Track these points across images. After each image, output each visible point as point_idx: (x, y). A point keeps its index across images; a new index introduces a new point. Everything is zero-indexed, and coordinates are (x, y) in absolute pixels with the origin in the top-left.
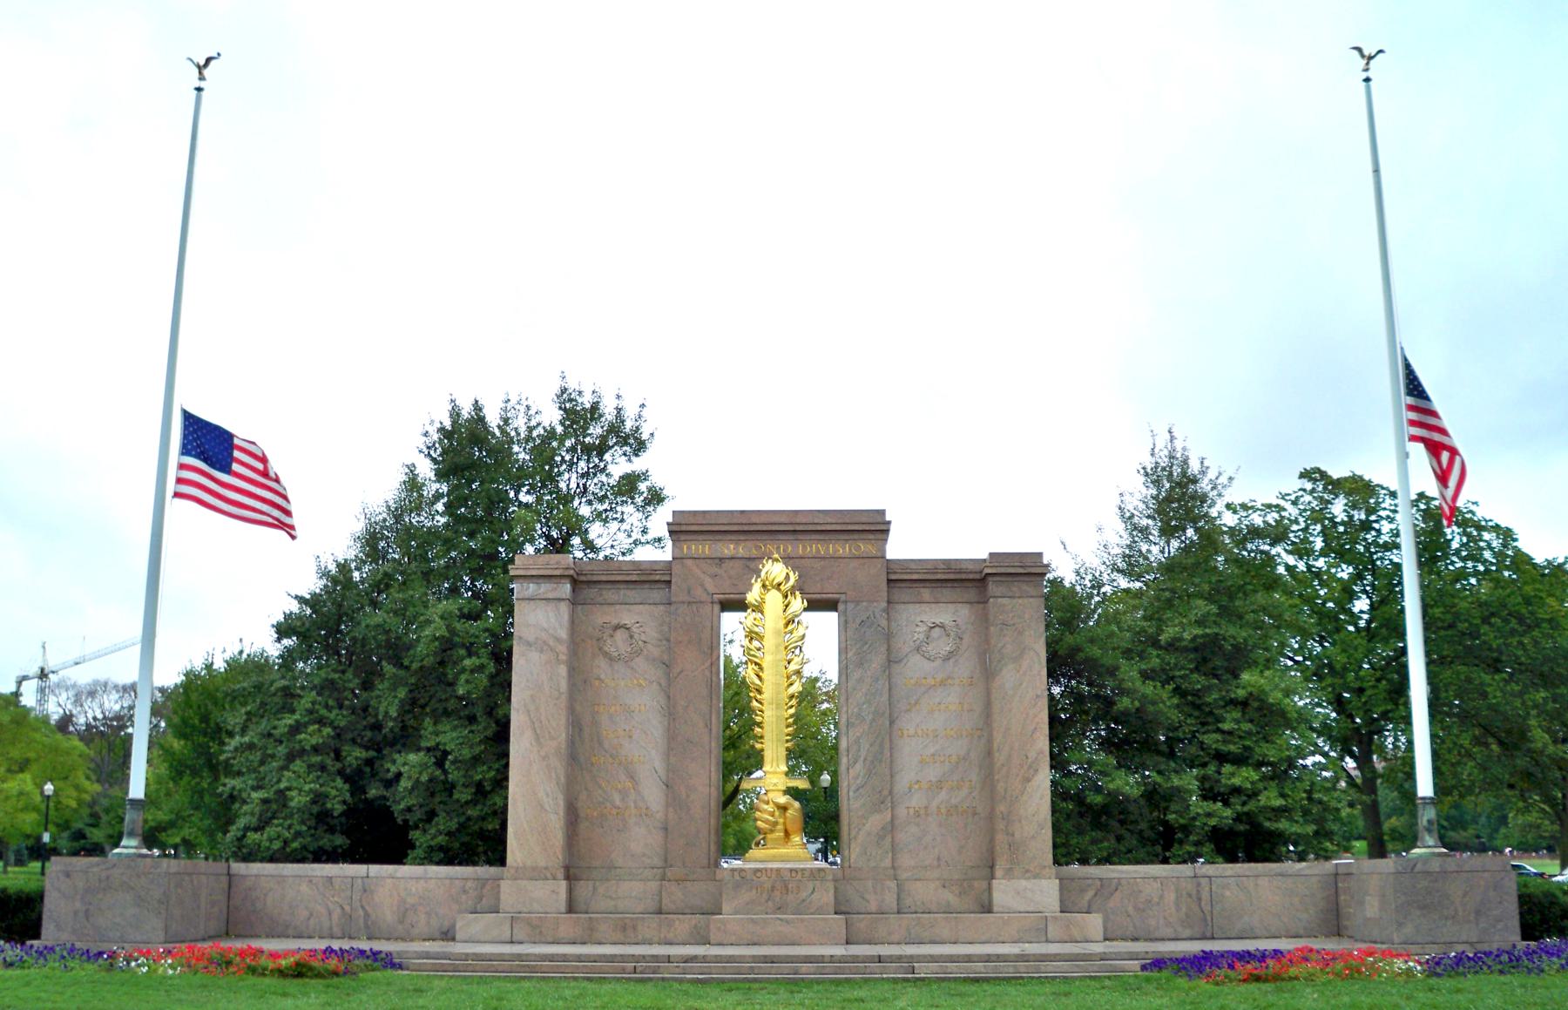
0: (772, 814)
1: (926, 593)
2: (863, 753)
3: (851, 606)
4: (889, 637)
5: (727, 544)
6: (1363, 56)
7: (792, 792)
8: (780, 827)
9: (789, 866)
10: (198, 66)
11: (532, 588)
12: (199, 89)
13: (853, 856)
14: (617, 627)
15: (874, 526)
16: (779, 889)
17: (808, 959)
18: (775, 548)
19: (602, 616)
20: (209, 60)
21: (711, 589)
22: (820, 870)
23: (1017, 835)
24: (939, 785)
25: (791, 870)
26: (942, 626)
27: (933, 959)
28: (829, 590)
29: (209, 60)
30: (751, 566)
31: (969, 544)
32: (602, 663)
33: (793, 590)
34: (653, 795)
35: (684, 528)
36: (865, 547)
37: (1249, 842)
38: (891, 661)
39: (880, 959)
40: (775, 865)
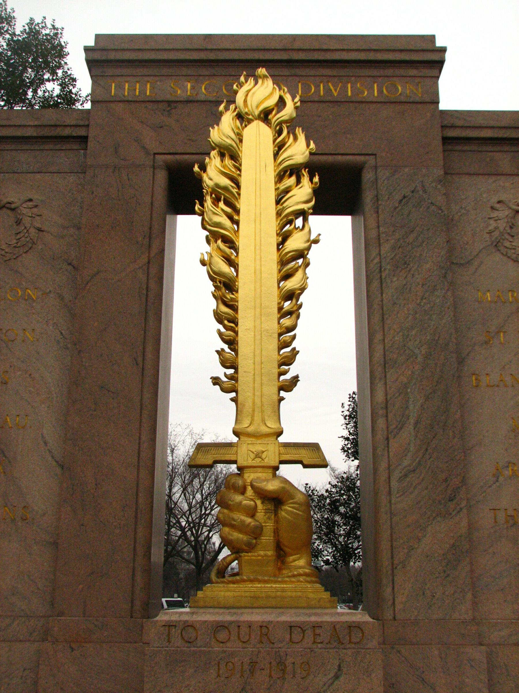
0: (252, 513)
2: (413, 411)
4: (449, 223)
8: (267, 538)
9: (287, 617)
13: (400, 599)
15: (423, 58)
21: (153, 146)
22: (352, 627)
25: (291, 627)
33: (292, 124)
35: (112, 56)
38: (453, 263)
40: (256, 617)
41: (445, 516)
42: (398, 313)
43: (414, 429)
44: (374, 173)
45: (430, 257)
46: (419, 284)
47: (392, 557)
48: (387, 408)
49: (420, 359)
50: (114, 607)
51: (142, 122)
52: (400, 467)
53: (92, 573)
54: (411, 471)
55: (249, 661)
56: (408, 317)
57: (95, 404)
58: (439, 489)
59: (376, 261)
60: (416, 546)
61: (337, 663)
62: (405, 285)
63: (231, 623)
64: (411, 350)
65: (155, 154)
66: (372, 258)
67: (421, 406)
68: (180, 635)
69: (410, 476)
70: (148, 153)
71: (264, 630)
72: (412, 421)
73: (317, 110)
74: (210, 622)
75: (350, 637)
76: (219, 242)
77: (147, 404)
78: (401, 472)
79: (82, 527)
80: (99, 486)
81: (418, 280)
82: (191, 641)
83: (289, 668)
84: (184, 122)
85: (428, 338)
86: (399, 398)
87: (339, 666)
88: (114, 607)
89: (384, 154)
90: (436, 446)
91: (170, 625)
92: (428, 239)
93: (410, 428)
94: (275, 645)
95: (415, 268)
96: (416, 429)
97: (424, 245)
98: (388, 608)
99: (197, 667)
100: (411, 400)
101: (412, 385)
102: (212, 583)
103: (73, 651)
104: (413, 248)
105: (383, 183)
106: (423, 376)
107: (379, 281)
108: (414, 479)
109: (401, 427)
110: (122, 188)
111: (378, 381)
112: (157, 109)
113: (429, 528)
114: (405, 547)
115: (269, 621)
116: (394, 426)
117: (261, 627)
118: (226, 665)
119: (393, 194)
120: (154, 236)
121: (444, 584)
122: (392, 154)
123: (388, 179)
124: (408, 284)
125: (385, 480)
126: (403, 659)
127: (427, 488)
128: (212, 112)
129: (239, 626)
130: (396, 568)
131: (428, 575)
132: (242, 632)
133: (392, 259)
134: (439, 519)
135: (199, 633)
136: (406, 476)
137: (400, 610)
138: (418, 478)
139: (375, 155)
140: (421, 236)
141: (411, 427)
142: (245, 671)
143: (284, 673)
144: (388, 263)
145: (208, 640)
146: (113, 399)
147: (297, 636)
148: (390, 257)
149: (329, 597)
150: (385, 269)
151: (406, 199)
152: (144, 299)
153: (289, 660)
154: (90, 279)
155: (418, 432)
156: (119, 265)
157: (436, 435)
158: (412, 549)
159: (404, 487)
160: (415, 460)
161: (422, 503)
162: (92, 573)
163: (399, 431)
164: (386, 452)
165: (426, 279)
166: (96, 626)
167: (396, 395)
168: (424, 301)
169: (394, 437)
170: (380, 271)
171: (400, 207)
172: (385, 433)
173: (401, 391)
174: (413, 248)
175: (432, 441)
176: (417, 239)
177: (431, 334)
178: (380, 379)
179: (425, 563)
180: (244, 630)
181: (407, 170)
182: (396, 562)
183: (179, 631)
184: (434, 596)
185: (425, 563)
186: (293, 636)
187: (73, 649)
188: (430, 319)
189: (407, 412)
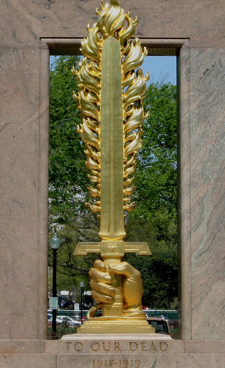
3: (194, 53)
13: (195, 327)
21: (39, 32)
28: (169, 33)
41: (223, 279)
42: (199, 151)
43: (207, 226)
44: (188, 52)
45: (222, 113)
46: (214, 132)
47: (191, 304)
48: (190, 213)
49: (212, 181)
50: (27, 333)
51: (31, 14)
52: (197, 250)
53: (14, 314)
54: (204, 252)
55: (109, 360)
56: (206, 154)
57: (10, 211)
58: (221, 263)
59: (186, 116)
60: (205, 297)
61: (154, 360)
62: (205, 132)
63: (100, 341)
64: (206, 175)
65: (41, 38)
66: (184, 113)
67: (212, 212)
68: (74, 347)
69: (203, 255)
70: (36, 38)
71: (117, 344)
72: (206, 221)
73: (151, 4)
74: (89, 340)
75: (161, 347)
76: (89, 119)
77: (42, 211)
78: (198, 253)
79: (6, 287)
80: (15, 262)
81: (213, 129)
82: (80, 350)
83: (130, 363)
84: (59, 14)
85: (218, 168)
86: (198, 207)
87: (155, 362)
88: (27, 333)
89: (195, 38)
90: (219, 237)
91: (68, 342)
92: (221, 100)
93: (204, 226)
94: (123, 352)
95: (212, 120)
96: (208, 226)
97: (218, 105)
98: (187, 333)
99: (83, 363)
100: (205, 208)
101: (206, 198)
102: (88, 320)
103: (5, 358)
104: (211, 107)
105: (193, 59)
106: (214, 192)
107: (188, 129)
108: (205, 257)
109: (198, 225)
110: (20, 64)
111: (185, 196)
112: (40, 3)
113: (213, 287)
114: (199, 298)
115: (119, 340)
116: (194, 225)
117: (115, 343)
118: (98, 362)
119: (200, 68)
120: (43, 98)
121: (221, 319)
122: (200, 38)
123: (197, 56)
124: (207, 131)
125: (188, 258)
126: (195, 361)
127: (213, 263)
128: (79, 6)
129: (104, 343)
130: (193, 310)
131: (211, 314)
132: (106, 346)
133: (197, 115)
134: (219, 281)
135: (84, 346)
136: (200, 255)
137: (194, 334)
138: (208, 256)
139: (189, 39)
140: (217, 98)
141: (205, 225)
142: (108, 364)
143: (127, 365)
144: (195, 117)
145: (88, 349)
146: (21, 208)
147: (134, 347)
148: (196, 113)
149: (151, 327)
150: (192, 121)
151: (208, 71)
152: (38, 142)
153: (129, 360)
154: (3, 129)
155: (209, 228)
156: (20, 119)
157: (220, 230)
158: (203, 299)
159: (199, 262)
160: (206, 245)
161: (210, 271)
162: (14, 314)
163: (197, 228)
164: (189, 240)
165: (219, 128)
166: (18, 344)
167: (196, 205)
168: (217, 143)
169: (194, 231)
170: (189, 122)
171: (204, 77)
172: (189, 229)
173: (199, 202)
174: (211, 107)
175: (217, 234)
176: (214, 100)
177: (220, 165)
178: (187, 195)
179: (210, 307)
180: (107, 344)
181: (210, 50)
182: (193, 306)
183: (73, 345)
184: (214, 326)
185: (210, 307)
186: (132, 347)
187: (5, 357)
188: (220, 155)
189: (202, 216)
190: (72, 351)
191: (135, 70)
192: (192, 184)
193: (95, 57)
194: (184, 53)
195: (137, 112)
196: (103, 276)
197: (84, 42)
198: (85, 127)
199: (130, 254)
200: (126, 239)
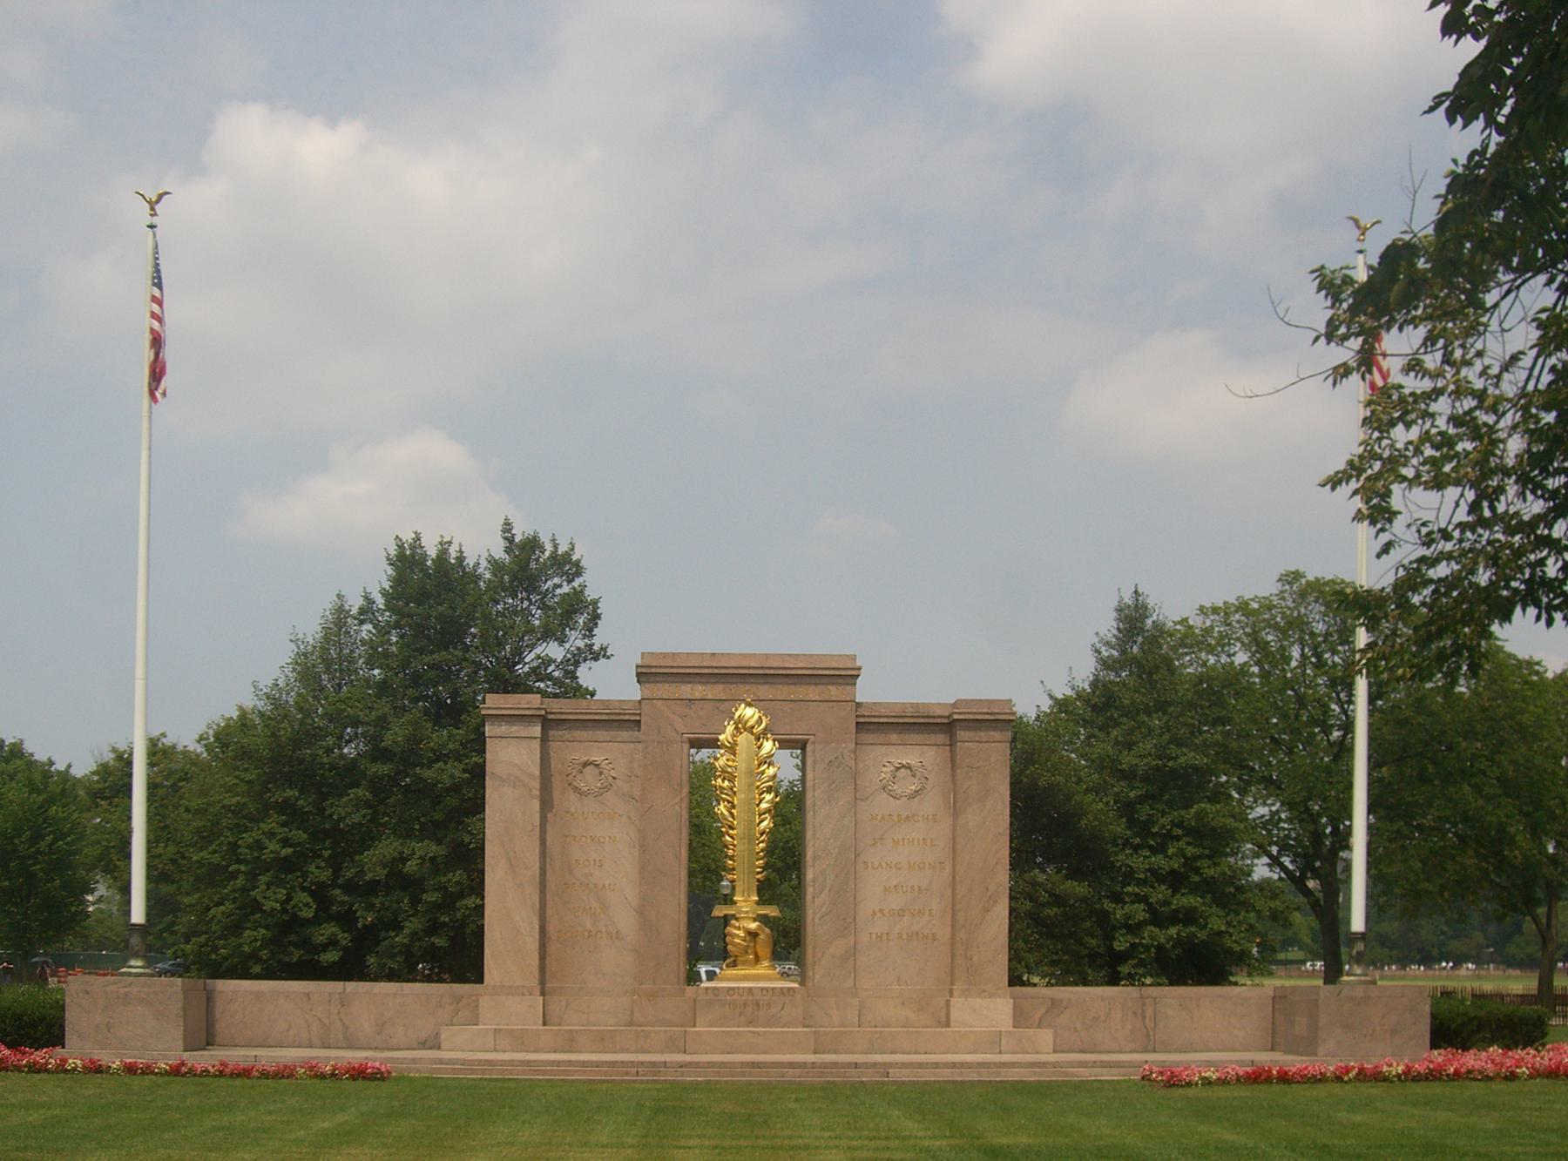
1: (894, 737)
3: (819, 747)
4: (855, 777)
5: (694, 683)
6: (1358, 227)
7: (763, 919)
9: (761, 985)
10: (149, 202)
11: (503, 729)
12: (151, 227)
14: (586, 764)
16: (751, 1007)
17: (792, 1065)
18: (742, 690)
19: (551, 733)
20: (160, 197)
23: (975, 959)
24: (901, 913)
26: (908, 767)
27: (903, 1065)
28: (798, 730)
29: (160, 197)
30: (724, 709)
31: (936, 689)
32: (573, 797)
34: (625, 920)
36: (834, 691)
37: (1201, 965)
39: (856, 1065)
190: (711, 996)
191: (768, 761)
192: (815, 858)
193: (732, 749)
194: (809, 748)
195: (768, 797)
196: (737, 934)
197: (721, 737)
198: (722, 809)
199: (1373, 872)
200: (758, 903)
